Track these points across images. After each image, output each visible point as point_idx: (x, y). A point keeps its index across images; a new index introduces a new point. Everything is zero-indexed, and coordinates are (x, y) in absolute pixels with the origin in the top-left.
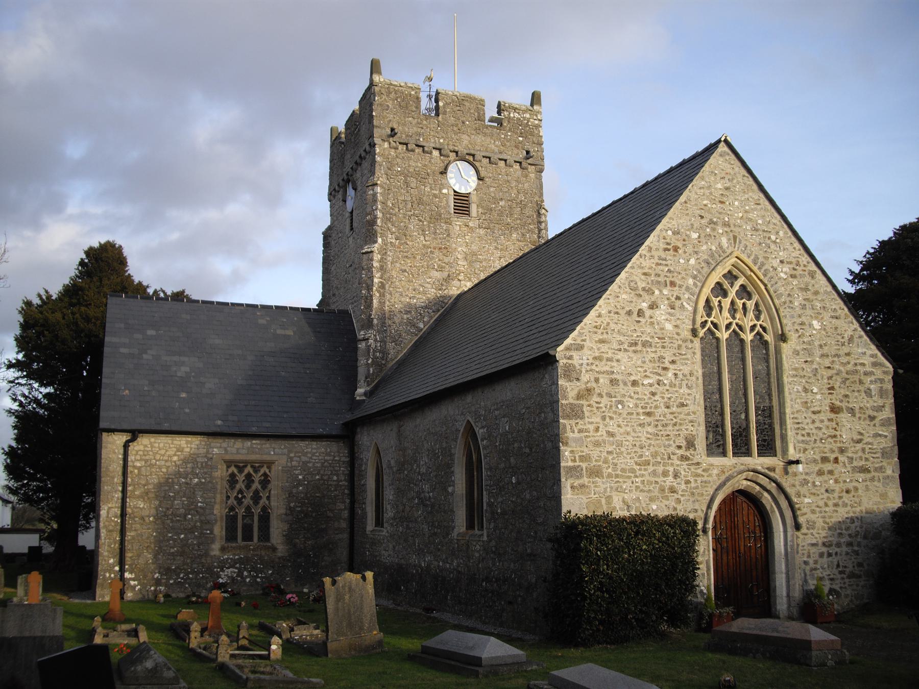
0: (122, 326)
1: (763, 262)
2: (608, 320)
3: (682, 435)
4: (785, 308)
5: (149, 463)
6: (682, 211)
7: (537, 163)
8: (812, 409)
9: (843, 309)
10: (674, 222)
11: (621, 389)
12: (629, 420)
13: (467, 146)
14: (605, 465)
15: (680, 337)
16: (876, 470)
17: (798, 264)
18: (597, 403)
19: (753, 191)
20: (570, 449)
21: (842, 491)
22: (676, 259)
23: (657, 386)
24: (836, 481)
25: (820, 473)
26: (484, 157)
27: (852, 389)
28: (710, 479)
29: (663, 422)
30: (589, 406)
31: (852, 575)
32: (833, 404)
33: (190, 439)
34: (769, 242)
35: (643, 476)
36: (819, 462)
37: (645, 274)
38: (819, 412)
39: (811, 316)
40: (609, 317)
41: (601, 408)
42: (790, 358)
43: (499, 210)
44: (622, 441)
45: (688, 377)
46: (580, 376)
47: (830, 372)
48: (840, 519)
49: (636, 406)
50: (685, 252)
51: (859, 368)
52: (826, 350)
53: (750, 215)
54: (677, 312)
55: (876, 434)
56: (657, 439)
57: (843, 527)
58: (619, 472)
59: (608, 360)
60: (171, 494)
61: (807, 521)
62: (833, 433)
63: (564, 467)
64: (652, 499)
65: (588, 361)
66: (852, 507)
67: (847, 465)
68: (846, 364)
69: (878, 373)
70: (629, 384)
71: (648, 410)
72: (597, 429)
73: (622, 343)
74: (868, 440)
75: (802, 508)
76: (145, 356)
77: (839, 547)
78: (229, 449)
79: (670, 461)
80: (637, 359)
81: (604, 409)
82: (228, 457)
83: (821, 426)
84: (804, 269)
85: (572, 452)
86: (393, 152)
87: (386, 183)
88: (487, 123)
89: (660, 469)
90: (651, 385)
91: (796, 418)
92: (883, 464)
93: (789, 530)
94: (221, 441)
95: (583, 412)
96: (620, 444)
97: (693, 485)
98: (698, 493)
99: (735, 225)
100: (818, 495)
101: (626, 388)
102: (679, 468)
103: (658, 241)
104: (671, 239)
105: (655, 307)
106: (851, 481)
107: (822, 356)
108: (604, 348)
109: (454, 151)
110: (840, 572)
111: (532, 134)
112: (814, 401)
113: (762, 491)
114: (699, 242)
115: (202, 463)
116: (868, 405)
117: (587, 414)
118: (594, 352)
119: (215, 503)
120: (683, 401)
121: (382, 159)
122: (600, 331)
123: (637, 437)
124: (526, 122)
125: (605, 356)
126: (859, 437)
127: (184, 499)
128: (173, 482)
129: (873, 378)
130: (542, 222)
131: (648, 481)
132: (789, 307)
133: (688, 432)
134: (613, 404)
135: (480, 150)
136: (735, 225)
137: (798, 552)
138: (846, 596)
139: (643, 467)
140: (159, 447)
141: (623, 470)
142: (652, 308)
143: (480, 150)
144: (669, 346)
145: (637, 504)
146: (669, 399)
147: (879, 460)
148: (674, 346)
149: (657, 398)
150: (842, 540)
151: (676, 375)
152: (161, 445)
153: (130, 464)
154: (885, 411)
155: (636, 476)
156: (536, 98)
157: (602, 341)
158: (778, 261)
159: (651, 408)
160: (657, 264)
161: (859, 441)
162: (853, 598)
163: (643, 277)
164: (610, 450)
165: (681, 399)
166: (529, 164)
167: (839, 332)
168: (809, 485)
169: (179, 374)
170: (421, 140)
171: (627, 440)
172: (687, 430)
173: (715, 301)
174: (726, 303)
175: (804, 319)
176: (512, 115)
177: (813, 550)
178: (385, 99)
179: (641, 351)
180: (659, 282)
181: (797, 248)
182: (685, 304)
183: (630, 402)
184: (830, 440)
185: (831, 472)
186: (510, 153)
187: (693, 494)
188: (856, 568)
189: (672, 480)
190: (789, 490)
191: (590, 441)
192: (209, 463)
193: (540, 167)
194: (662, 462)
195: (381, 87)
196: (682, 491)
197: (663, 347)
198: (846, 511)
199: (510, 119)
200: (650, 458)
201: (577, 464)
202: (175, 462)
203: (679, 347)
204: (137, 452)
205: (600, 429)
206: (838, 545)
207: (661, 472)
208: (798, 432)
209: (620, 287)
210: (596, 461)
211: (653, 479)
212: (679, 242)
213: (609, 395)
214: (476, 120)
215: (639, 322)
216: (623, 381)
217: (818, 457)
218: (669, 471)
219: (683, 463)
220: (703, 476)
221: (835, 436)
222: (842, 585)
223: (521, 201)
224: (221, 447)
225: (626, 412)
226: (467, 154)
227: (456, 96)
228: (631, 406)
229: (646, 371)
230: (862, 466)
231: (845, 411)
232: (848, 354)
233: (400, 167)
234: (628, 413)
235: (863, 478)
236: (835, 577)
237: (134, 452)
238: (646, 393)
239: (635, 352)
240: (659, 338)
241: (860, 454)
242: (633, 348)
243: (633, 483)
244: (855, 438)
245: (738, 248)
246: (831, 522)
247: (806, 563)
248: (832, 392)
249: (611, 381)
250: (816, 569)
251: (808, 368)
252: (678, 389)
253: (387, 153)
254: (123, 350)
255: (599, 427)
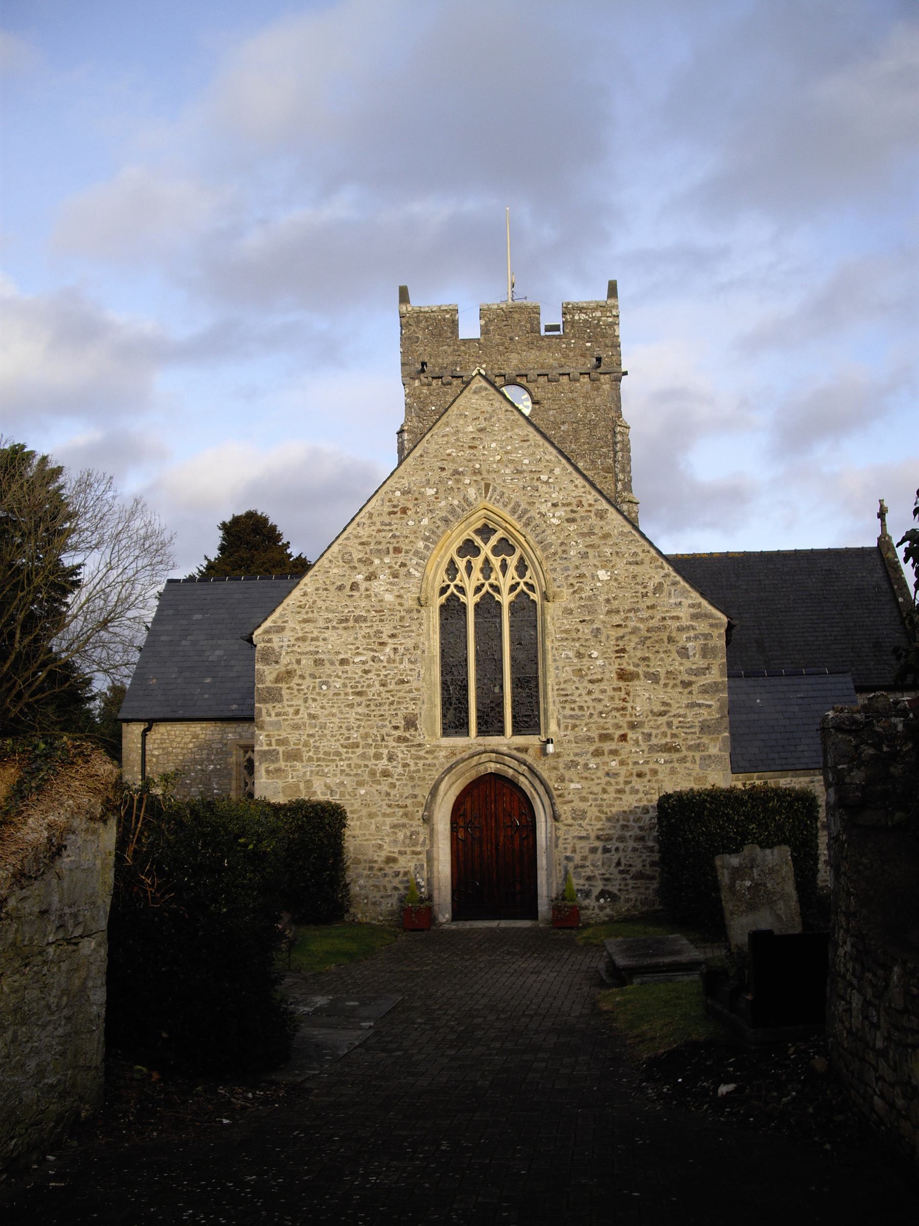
0: (171, 612)
1: (525, 509)
2: (314, 597)
3: (400, 715)
4: (555, 560)
5: (166, 751)
6: (416, 466)
7: (610, 370)
8: (589, 678)
9: (648, 552)
10: (403, 481)
11: (327, 669)
12: (335, 701)
13: (517, 366)
14: (304, 749)
15: (404, 608)
16: (690, 748)
17: (580, 504)
18: (298, 685)
19: (520, 426)
20: (266, 733)
21: (631, 774)
22: (404, 522)
23: (372, 663)
24: (622, 763)
25: (597, 753)
26: (539, 375)
27: (655, 649)
28: (434, 761)
29: (377, 702)
30: (288, 688)
31: (639, 876)
32: (622, 670)
33: (204, 725)
34: (536, 483)
35: (349, 759)
36: (597, 740)
37: (362, 544)
38: (601, 680)
39: (595, 565)
40: (316, 594)
41: (302, 690)
42: (558, 619)
43: (561, 436)
44: (326, 723)
45: (412, 651)
46: (280, 658)
47: (621, 632)
48: (626, 809)
49: (345, 685)
50: (417, 513)
51: (669, 622)
52: (615, 604)
53: (513, 456)
54: (401, 581)
55: (692, 703)
56: (369, 720)
57: (631, 818)
58: (321, 756)
59: (313, 639)
60: (188, 782)
61: (573, 810)
62: (619, 704)
63: (258, 751)
64: (360, 784)
65: (289, 643)
66: (645, 795)
67: (641, 743)
68: (647, 619)
69: (702, 627)
70: (337, 663)
71: (359, 689)
72: (297, 712)
73: (330, 621)
74: (677, 712)
75: (566, 795)
76: (184, 643)
77: (622, 842)
78: (243, 734)
79: (384, 743)
80: (347, 636)
81: (306, 691)
82: (242, 742)
83: (601, 697)
84: (589, 509)
85: (268, 736)
86: (425, 390)
87: (418, 427)
88: (543, 333)
89: (372, 751)
90: (364, 663)
91: (562, 689)
92: (702, 740)
93: (549, 820)
94: (235, 725)
95: (281, 695)
96: (323, 727)
97: (412, 768)
98: (419, 778)
99: (488, 472)
100: (592, 780)
101: (333, 668)
102: (395, 750)
103: (382, 505)
104: (399, 501)
105: (373, 578)
106: (647, 762)
107: (609, 612)
108: (308, 627)
109: (501, 375)
110: (621, 872)
111: (604, 336)
112: (592, 667)
113: (516, 774)
114: (437, 498)
115: (217, 749)
116: (682, 668)
117: (285, 697)
118: (297, 633)
119: (231, 789)
120: (403, 677)
121: (412, 400)
122: (304, 611)
123: (344, 718)
124: (596, 322)
125: (310, 636)
126: (663, 708)
127: (201, 786)
128: (189, 770)
129: (692, 634)
130: (618, 442)
131: (355, 764)
132: (561, 558)
133: (408, 711)
134: (317, 685)
135: (534, 369)
136: (488, 472)
137: (557, 846)
138: (628, 900)
139: (350, 750)
140: (175, 735)
141: (326, 753)
142: (370, 580)
143: (534, 369)
144: (389, 618)
145: (342, 789)
146: (386, 676)
147: (694, 736)
148: (396, 618)
149: (370, 676)
150: (628, 834)
151: (395, 650)
152: (178, 733)
153: (148, 752)
154: (710, 673)
155: (341, 760)
156: (613, 290)
157: (306, 621)
158: (550, 504)
159: (362, 687)
160: (379, 531)
161: (662, 714)
162: (638, 903)
163: (360, 547)
164: (311, 733)
165: (401, 675)
166: (600, 373)
167: (639, 580)
168: (579, 767)
169: (211, 659)
170: (458, 369)
171: (333, 722)
172: (407, 708)
173: (461, 563)
174: (478, 563)
175: (584, 570)
176: (576, 318)
177: (580, 844)
178: (414, 331)
179: (352, 627)
180: (379, 551)
181: (580, 485)
182: (412, 570)
183: (336, 681)
184: (614, 713)
185: (614, 752)
186: (574, 364)
187: (412, 778)
188: (648, 867)
189: (386, 763)
190: (545, 775)
191: (288, 724)
192: (224, 749)
193: (615, 374)
194: (374, 744)
195: (409, 317)
196: (398, 775)
197: (381, 621)
198: (636, 799)
199: (574, 323)
200: (359, 740)
201: (274, 747)
202: (191, 749)
203: (402, 619)
204: (155, 740)
205: (301, 712)
206: (621, 839)
207: (372, 755)
208: (565, 705)
209: (331, 561)
210: (294, 744)
211: (362, 763)
212: (409, 503)
213: (313, 676)
214: (528, 333)
215: (352, 596)
216: (329, 660)
217: (595, 734)
218: (383, 754)
219: (400, 745)
220: (427, 759)
221: (624, 709)
222: (622, 887)
223: (590, 421)
224: (235, 732)
225: (332, 693)
226: (517, 376)
227: (501, 309)
228: (338, 686)
229: (358, 648)
230: (667, 744)
231: (642, 677)
232: (652, 607)
233: (434, 406)
234: (334, 694)
235: (667, 758)
236: (612, 876)
237: (152, 741)
238: (357, 671)
239: (345, 628)
240: (376, 611)
241: (664, 728)
242: (344, 625)
243: (337, 766)
244: (655, 710)
245: (491, 497)
246: (611, 811)
247: (568, 859)
248: (622, 655)
249: (315, 661)
250: (583, 866)
251: (586, 630)
252: (398, 665)
253: (418, 392)
254: (163, 638)
255: (299, 710)
